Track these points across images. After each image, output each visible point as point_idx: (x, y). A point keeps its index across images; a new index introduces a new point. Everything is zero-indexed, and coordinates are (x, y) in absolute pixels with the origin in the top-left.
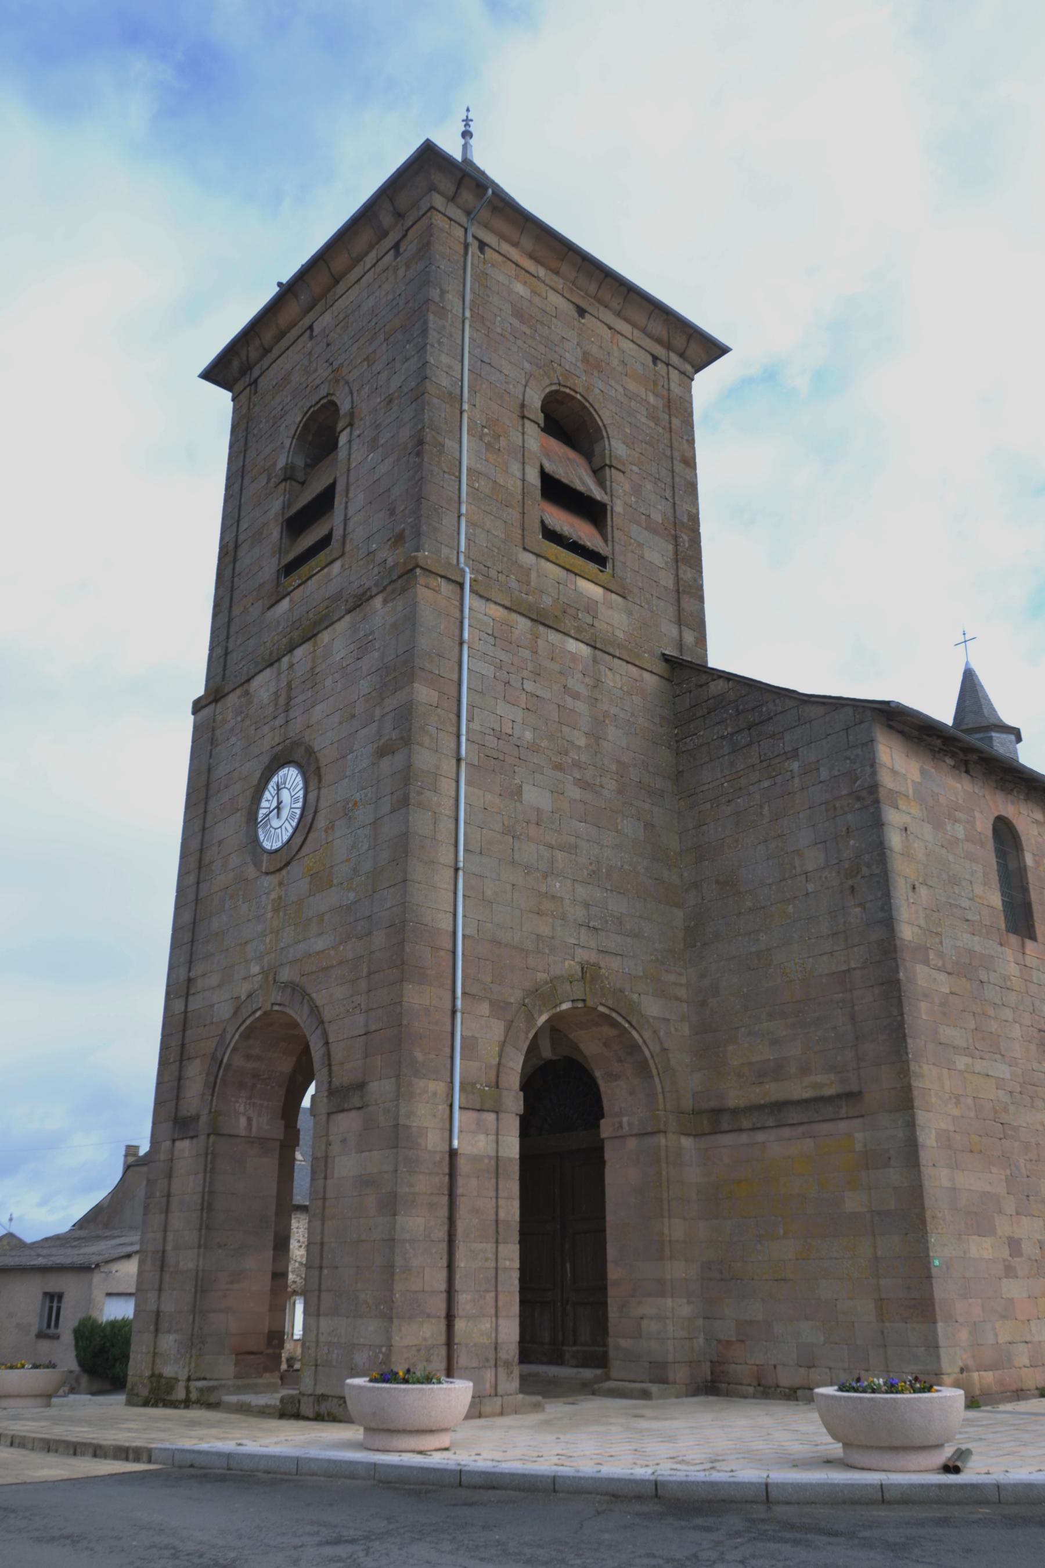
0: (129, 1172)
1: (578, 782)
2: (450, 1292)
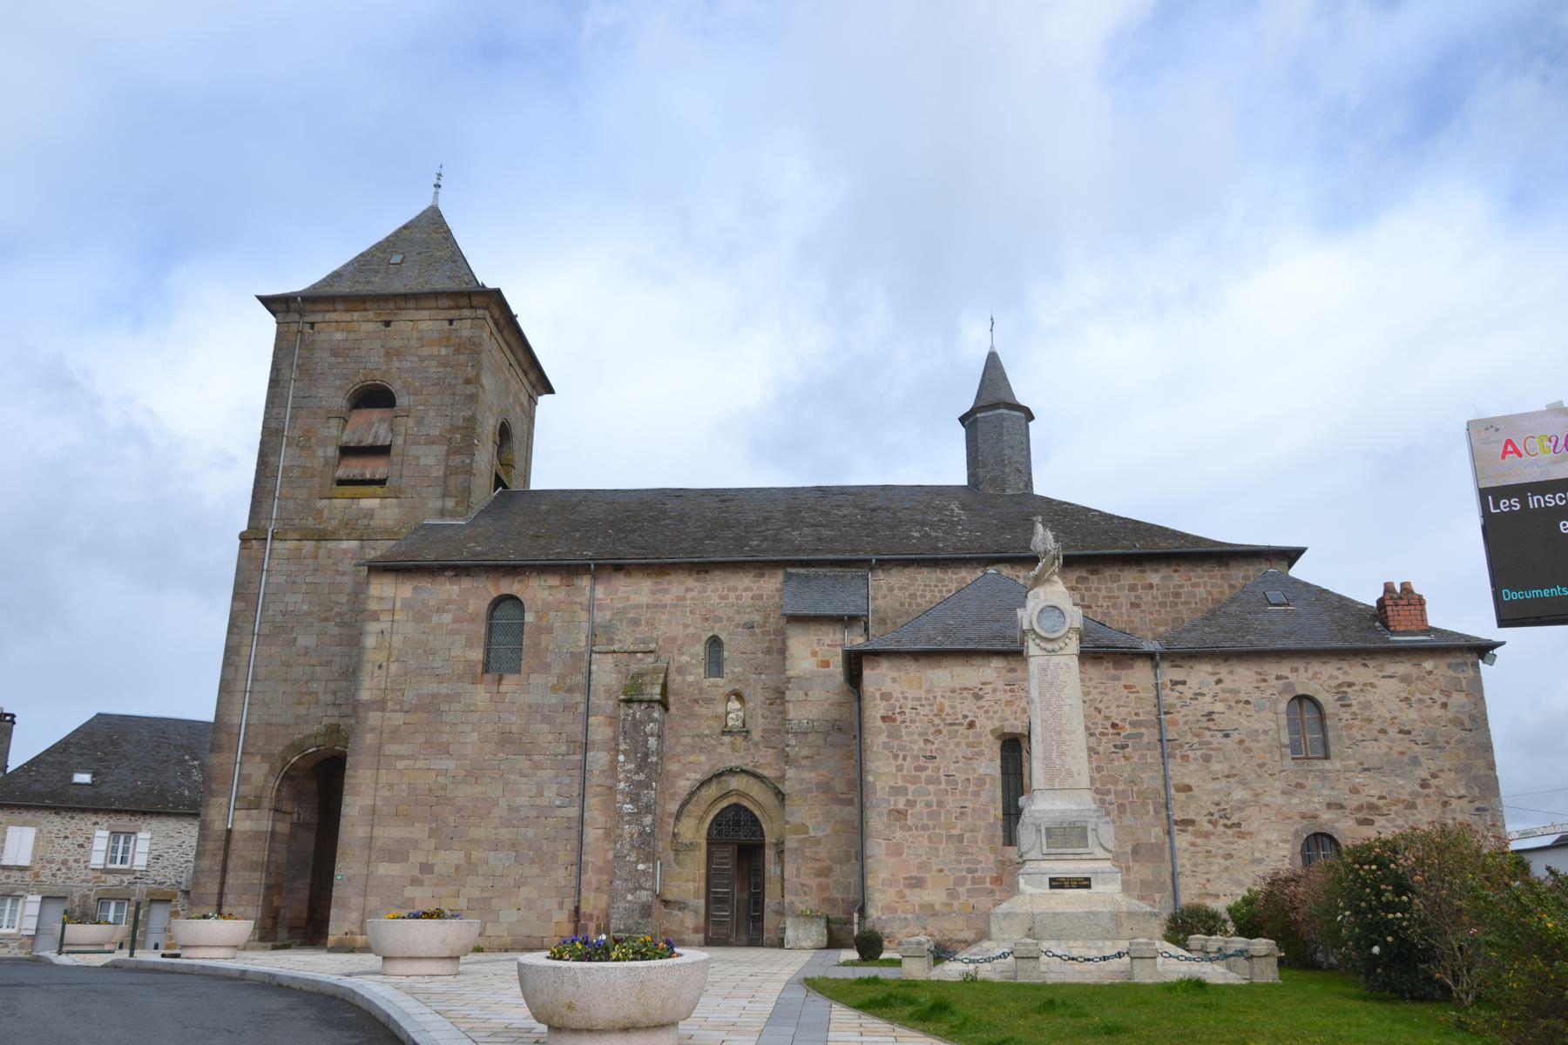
0: (497, 614)
1: (337, 624)
2: (221, 894)
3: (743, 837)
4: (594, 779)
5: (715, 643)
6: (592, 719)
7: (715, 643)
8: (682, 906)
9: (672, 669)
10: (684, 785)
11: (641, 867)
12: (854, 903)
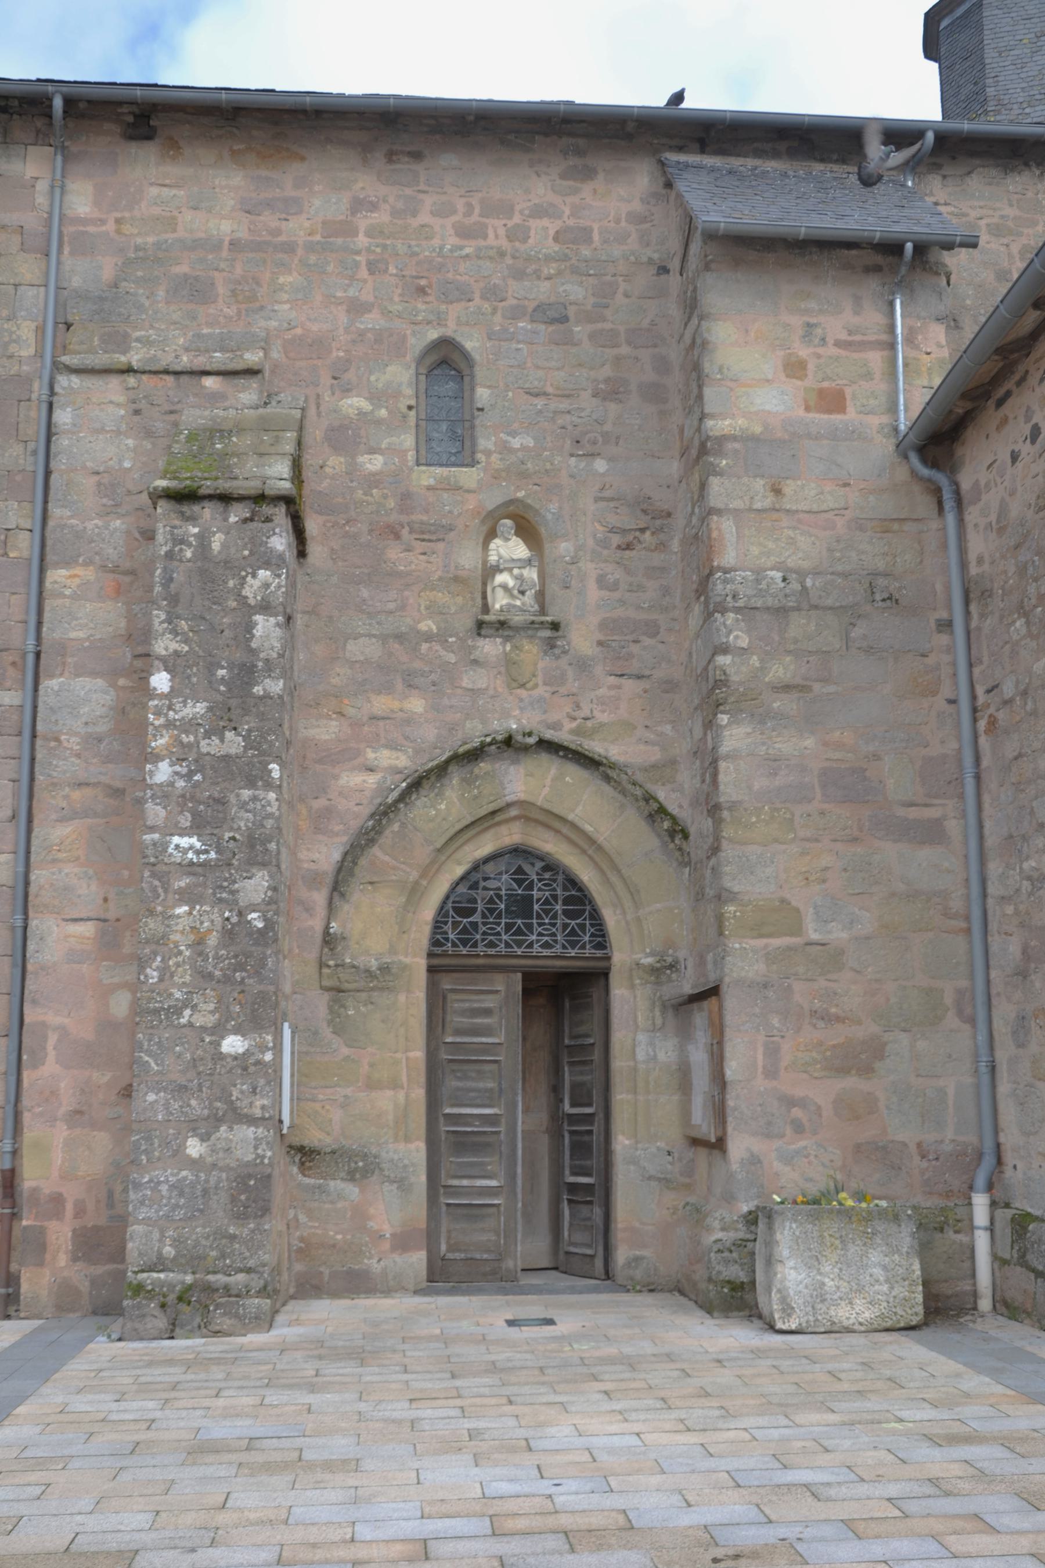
3: (548, 949)
4: (65, 764)
5: (446, 362)
6: (56, 576)
7: (446, 362)
8: (360, 1166)
9: (315, 433)
10: (357, 788)
11: (233, 1044)
12: (967, 1161)
